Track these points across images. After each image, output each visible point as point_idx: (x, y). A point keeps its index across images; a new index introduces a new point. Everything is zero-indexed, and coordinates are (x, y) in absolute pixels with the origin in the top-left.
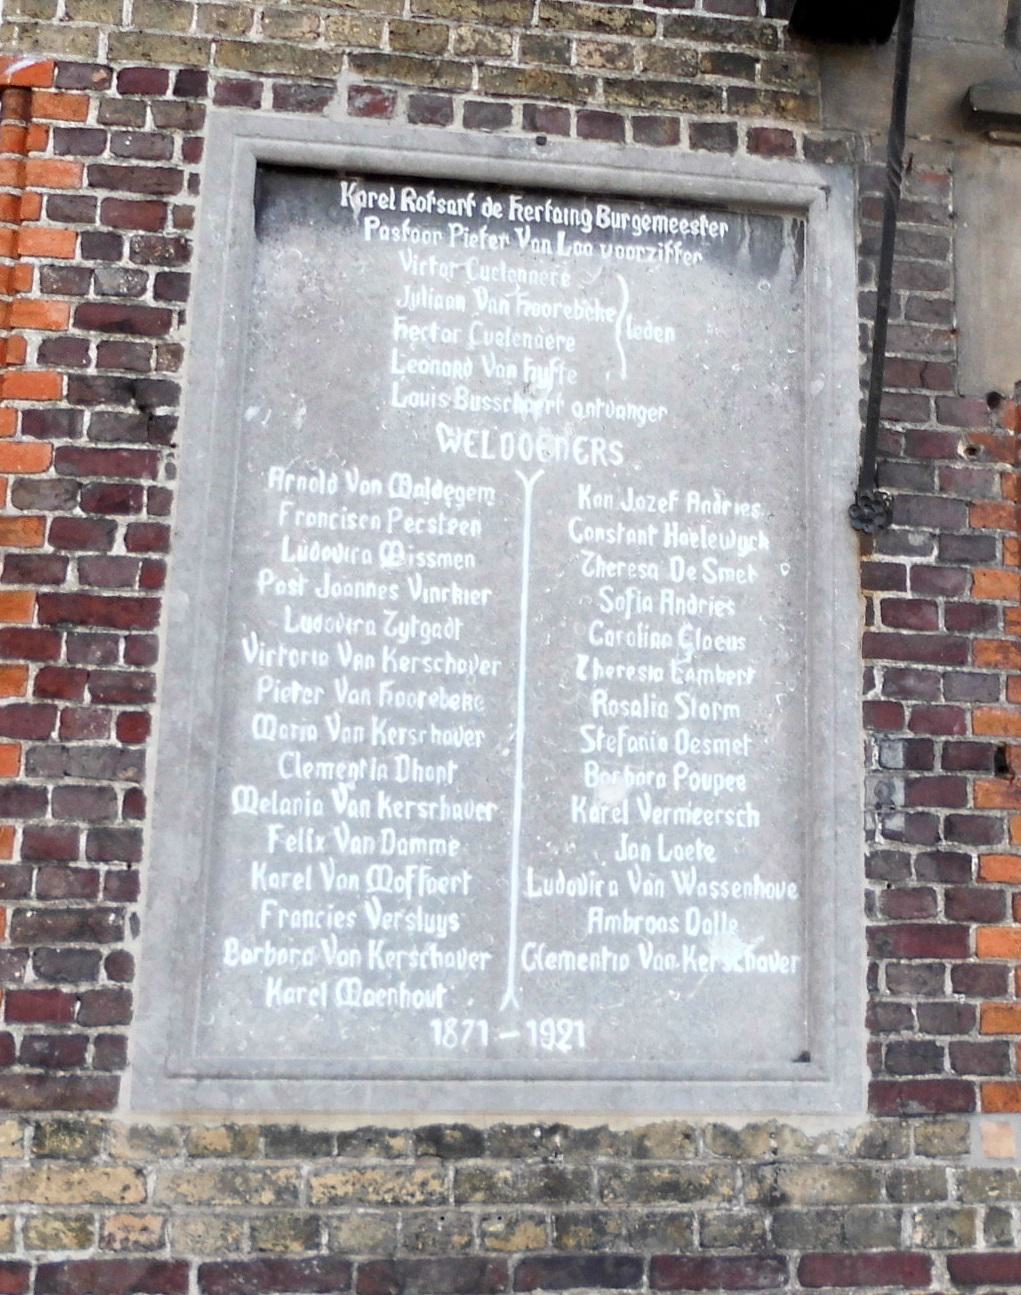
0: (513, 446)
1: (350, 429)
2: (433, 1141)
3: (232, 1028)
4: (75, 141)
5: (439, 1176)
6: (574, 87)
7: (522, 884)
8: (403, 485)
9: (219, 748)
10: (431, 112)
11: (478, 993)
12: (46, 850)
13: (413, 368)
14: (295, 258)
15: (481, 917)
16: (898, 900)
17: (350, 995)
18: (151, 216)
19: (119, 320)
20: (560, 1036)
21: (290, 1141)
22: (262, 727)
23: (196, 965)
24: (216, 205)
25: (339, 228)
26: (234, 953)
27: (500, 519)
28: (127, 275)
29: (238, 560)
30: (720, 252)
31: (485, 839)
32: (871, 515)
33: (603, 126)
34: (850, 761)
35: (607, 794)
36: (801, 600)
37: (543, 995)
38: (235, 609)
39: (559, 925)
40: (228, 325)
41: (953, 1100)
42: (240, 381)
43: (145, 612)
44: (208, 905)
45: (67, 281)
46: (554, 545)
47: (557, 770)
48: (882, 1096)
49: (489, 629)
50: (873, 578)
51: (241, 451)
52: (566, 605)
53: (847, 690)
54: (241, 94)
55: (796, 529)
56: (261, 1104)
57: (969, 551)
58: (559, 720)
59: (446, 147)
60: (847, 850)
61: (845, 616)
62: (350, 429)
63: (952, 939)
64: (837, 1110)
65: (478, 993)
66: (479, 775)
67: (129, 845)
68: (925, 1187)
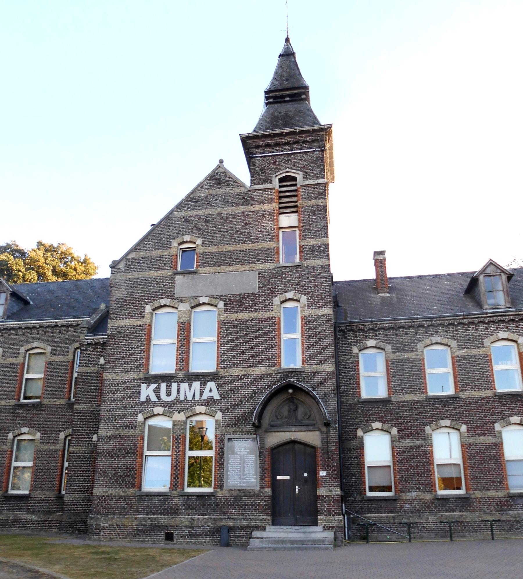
0: (242, 453)
1: (233, 453)
2: (238, 490)
3: (229, 485)
4: (219, 438)
5: (238, 492)
6: (244, 432)
7: (242, 477)
8: (236, 456)
9: (228, 471)
10: (236, 435)
11: (240, 483)
12: (220, 476)
13: (236, 449)
14: (230, 443)
15: (240, 479)
16: (261, 477)
17: (234, 483)
18: (222, 442)
19: (222, 448)
20: (244, 485)
21: (232, 490)
22: (230, 469)
23: (227, 482)
24: (226, 441)
25: (64, 249)
26: (229, 481)
27: (241, 457)
28: (222, 446)
29: (228, 460)
30: (252, 441)
31: (240, 475)
32: (260, 456)
33: (245, 434)
34: (259, 470)
35: (246, 472)
36: (256, 460)
37: (244, 483)
38: (228, 463)
39: (244, 479)
40: (14, 301)
41: (264, 488)
42: (227, 451)
43: (223, 464)
44: (227, 479)
45: (219, 446)
46: (244, 459)
47: (244, 471)
48: (260, 488)
49: (240, 464)
50: (260, 459)
51: (228, 455)
52: (244, 462)
53: (259, 466)
54: (227, 435)
55: (256, 456)
56: (230, 488)
57: (265, 457)
58: (244, 468)
59: (237, 436)
60: (259, 474)
61: (258, 462)
62: (233, 453)
63: (264, 479)
64: (258, 488)
65: (240, 483)
66: (240, 471)
67: (223, 476)
68: (262, 492)
